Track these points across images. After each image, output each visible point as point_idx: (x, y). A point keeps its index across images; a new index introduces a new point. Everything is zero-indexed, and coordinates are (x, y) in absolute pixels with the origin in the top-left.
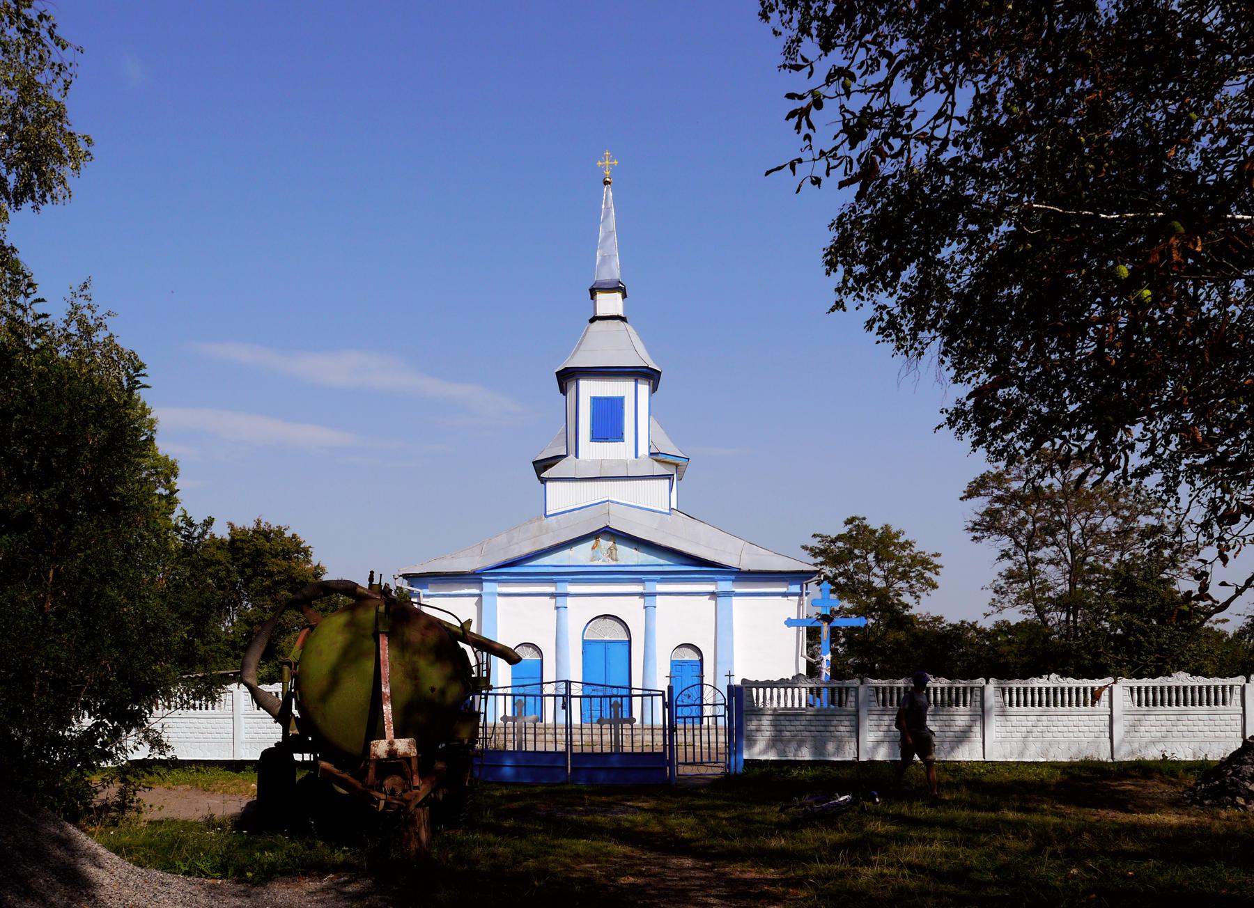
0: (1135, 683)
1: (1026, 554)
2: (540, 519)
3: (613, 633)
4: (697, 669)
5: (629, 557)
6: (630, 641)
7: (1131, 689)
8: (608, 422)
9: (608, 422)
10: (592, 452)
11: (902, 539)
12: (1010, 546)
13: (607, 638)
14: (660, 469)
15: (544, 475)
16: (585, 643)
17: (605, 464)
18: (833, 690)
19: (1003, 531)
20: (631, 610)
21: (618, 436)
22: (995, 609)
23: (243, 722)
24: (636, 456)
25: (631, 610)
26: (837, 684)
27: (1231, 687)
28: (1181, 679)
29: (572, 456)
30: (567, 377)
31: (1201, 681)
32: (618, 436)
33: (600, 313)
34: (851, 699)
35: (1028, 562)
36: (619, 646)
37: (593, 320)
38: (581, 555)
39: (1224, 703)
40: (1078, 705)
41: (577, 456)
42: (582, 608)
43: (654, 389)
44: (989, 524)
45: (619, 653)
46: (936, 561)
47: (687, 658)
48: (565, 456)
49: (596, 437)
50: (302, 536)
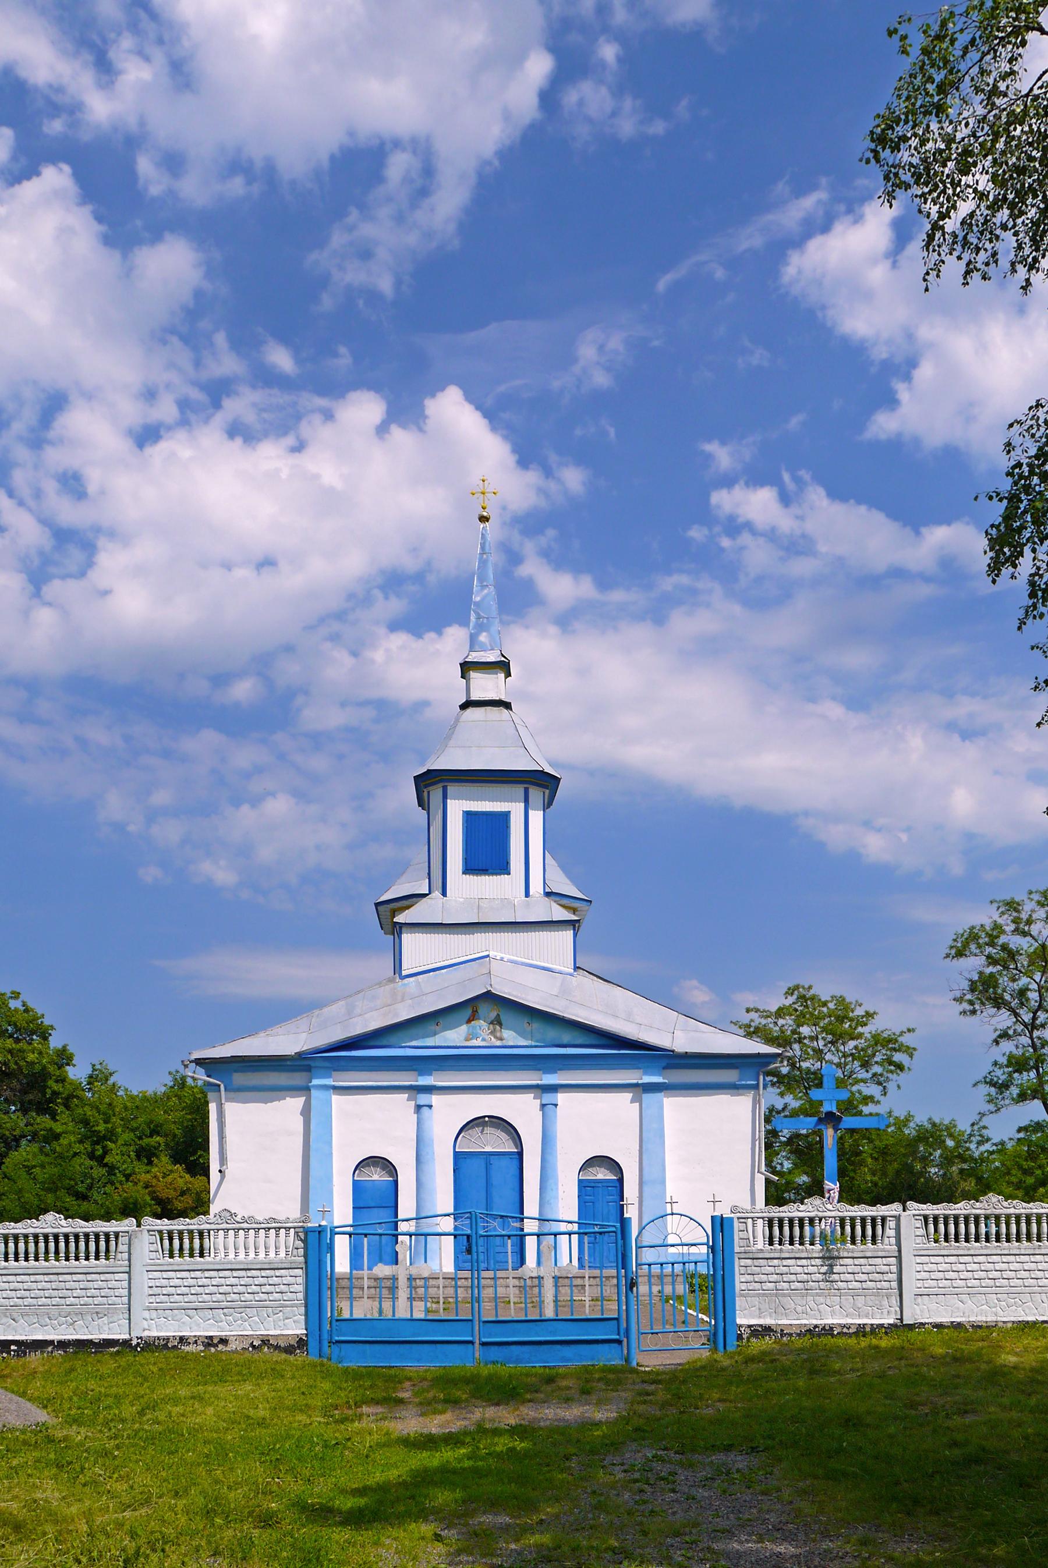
0: (164, 1224)
1: (1031, 1033)
2: (391, 981)
3: (495, 1142)
4: (615, 1191)
5: (513, 1039)
6: (520, 1154)
7: (926, 1218)
8: (487, 850)
9: (487, 850)
10: (468, 892)
11: (859, 1012)
12: (1009, 1023)
13: (488, 1149)
14: (560, 914)
15: (400, 918)
16: (457, 1156)
17: (484, 904)
18: (770, 1222)
19: (998, 1003)
20: (521, 1110)
21: (503, 868)
22: (992, 1107)
23: (142, 1280)
24: (527, 895)
25: (521, 1110)
26: (776, 1212)
27: (884, 1219)
28: (51, 1223)
29: (437, 894)
30: (431, 783)
31: (80, 1226)
32: (503, 868)
33: (475, 696)
34: (123, 1248)
35: (1034, 1046)
36: (504, 1162)
37: (464, 706)
38: (454, 1037)
39: (874, 1241)
40: (967, 1240)
41: (444, 894)
42: (450, 1113)
43: (548, 804)
44: (985, 992)
45: (503, 1170)
46: (906, 1040)
47: (600, 1176)
48: (424, 895)
49: (471, 868)
50: (38, 1007)
